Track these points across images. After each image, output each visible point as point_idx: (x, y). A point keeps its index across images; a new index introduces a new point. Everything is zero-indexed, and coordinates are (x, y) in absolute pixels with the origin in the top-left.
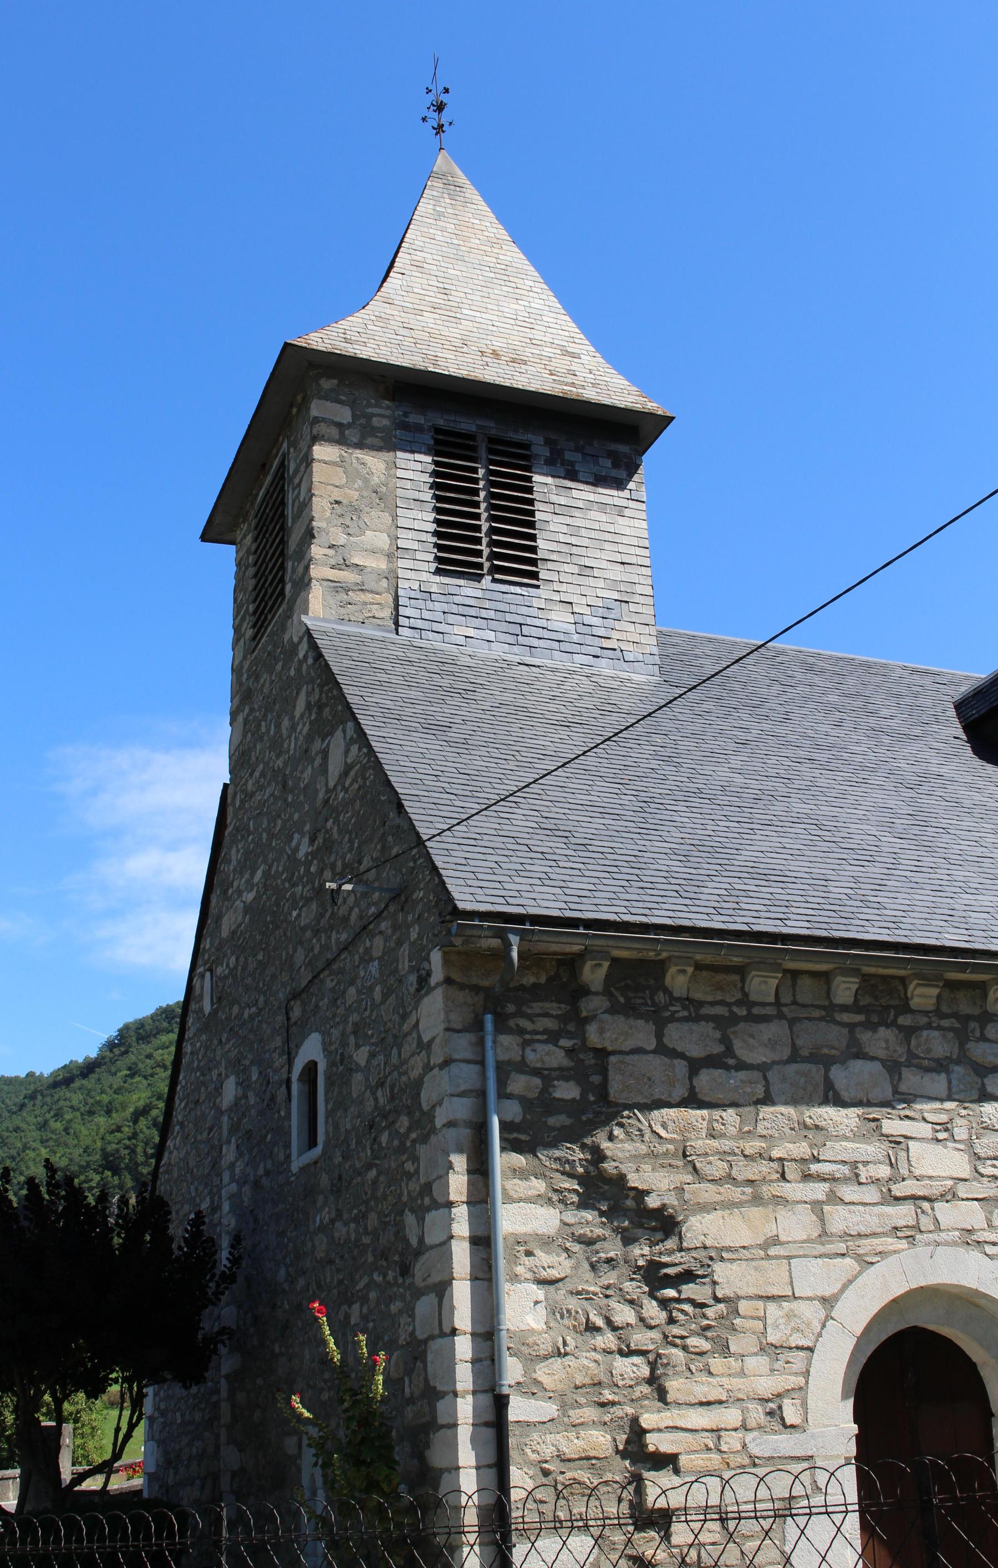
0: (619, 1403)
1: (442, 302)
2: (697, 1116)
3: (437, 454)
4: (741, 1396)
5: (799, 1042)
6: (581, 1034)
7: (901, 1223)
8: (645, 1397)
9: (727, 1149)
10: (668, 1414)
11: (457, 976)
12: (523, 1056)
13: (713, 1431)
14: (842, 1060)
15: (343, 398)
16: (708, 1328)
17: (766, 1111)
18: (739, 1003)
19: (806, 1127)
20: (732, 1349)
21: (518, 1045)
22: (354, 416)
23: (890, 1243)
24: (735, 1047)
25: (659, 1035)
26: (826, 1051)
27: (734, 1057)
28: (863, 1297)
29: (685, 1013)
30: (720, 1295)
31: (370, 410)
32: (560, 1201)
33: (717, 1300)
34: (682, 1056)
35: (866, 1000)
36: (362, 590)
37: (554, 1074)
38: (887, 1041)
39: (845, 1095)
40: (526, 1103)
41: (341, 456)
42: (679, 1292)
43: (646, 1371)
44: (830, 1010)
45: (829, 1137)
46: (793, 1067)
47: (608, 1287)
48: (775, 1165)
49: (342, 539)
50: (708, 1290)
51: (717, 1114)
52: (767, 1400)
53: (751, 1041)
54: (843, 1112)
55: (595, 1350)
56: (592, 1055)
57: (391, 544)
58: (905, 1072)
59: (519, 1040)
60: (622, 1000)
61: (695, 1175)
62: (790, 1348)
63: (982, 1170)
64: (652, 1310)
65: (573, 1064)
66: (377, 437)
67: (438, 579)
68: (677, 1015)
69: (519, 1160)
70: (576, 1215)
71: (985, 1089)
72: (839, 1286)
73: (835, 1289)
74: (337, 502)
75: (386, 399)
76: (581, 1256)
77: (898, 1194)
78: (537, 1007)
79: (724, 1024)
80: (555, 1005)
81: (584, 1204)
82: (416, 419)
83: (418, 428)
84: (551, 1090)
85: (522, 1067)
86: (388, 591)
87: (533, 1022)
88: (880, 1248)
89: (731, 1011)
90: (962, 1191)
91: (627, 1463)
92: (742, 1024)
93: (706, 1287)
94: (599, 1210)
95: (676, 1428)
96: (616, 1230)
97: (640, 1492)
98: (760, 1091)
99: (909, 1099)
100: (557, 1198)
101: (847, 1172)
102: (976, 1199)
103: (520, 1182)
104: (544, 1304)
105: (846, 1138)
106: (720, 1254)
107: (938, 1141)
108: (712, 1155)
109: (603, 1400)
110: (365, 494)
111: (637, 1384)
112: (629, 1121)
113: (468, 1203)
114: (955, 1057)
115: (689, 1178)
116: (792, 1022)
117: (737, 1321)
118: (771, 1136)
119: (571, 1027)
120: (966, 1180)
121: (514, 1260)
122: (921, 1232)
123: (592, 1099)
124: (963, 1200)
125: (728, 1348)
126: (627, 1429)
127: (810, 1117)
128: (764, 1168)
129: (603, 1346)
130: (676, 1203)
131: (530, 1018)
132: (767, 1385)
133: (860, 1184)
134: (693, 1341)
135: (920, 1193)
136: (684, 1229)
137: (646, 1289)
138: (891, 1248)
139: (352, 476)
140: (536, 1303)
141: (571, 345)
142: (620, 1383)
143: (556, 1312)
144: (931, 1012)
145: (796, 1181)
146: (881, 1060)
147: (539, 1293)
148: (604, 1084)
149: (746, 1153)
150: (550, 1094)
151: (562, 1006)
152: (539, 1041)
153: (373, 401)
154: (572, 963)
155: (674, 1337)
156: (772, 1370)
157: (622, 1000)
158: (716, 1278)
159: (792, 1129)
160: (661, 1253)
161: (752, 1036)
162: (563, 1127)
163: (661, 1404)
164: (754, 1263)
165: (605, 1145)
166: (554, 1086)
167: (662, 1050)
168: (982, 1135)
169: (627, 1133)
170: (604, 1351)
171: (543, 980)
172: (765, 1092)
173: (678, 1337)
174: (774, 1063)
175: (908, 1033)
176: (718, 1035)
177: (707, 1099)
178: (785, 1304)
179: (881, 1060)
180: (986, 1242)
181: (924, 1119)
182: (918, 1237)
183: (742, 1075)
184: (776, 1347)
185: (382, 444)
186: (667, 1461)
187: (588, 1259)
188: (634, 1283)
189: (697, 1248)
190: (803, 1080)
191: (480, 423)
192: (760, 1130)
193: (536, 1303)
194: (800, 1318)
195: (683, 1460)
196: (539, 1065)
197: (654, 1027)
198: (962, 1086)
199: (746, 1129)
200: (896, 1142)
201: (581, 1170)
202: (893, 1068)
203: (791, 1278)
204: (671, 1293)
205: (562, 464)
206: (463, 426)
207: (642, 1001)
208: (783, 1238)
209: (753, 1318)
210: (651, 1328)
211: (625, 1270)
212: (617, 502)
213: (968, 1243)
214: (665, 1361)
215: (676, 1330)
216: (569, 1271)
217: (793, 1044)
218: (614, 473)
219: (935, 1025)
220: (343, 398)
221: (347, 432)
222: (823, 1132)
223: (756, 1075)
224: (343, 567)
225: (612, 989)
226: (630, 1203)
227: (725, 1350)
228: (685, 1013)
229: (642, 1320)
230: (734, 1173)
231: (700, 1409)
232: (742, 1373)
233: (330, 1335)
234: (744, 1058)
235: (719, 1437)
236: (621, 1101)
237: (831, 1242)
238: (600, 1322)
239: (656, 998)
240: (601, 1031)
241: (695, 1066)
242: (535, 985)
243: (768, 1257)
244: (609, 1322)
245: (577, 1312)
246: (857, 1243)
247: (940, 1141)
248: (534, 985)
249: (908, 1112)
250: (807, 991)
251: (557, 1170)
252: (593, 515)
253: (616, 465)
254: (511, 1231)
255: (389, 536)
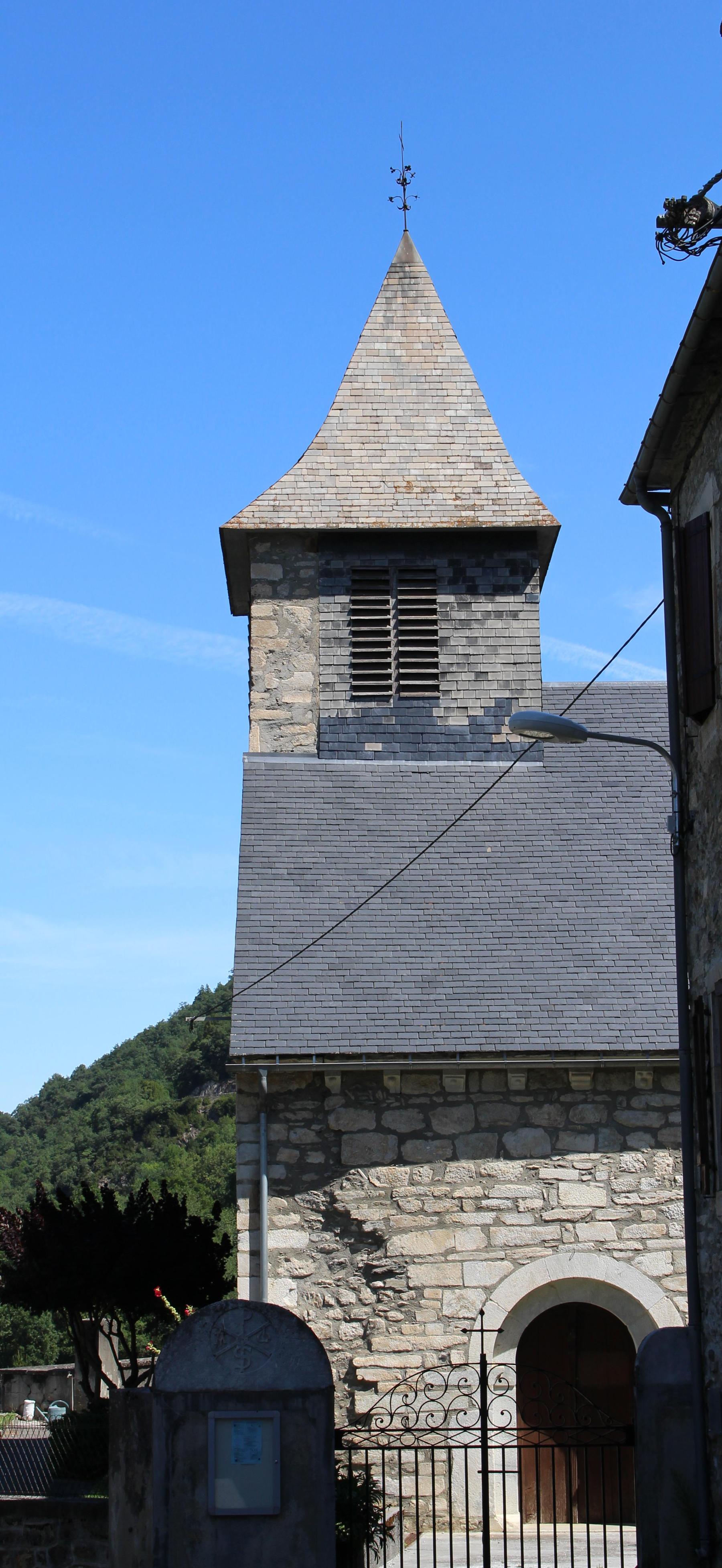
0: (342, 1350)
1: (371, 433)
2: (402, 1171)
3: (354, 592)
4: (421, 1348)
5: (481, 1118)
6: (325, 1121)
7: (549, 1237)
8: (359, 1347)
9: (421, 1192)
10: (372, 1358)
11: (245, 1088)
12: (288, 1137)
13: (401, 1368)
14: (514, 1129)
15: (275, 558)
16: (402, 1305)
17: (453, 1165)
18: (437, 1094)
19: (482, 1176)
20: (418, 1318)
21: (285, 1130)
22: (285, 573)
23: (539, 1251)
24: (433, 1124)
25: (378, 1120)
26: (501, 1123)
27: (432, 1130)
28: (515, 1286)
29: (397, 1104)
30: (411, 1285)
31: (298, 564)
32: (309, 1227)
33: (410, 1288)
34: (394, 1132)
35: (534, 1086)
36: (291, 724)
37: (309, 1147)
38: (549, 1114)
39: (513, 1152)
40: (288, 1166)
41: (274, 611)
42: (385, 1283)
43: (361, 1331)
44: (506, 1095)
45: (498, 1182)
46: (476, 1135)
47: (339, 1280)
48: (456, 1202)
49: (275, 683)
50: (404, 1281)
51: (416, 1169)
52: (441, 1351)
53: (445, 1119)
54: (511, 1164)
55: (328, 1318)
56: (332, 1134)
57: (315, 681)
58: (562, 1135)
59: (285, 1126)
60: (353, 1098)
61: (399, 1210)
62: (459, 1318)
63: (616, 1200)
64: (367, 1294)
65: (321, 1140)
66: (304, 587)
67: (353, 705)
68: (391, 1106)
69: (283, 1202)
70: (319, 1236)
71: (626, 1144)
72: (497, 1279)
73: (494, 1281)
74: (271, 652)
75: (310, 551)
76: (323, 1261)
77: (547, 1218)
78: (299, 1104)
79: (426, 1110)
80: (310, 1102)
81: (326, 1228)
82: (337, 564)
83: (339, 573)
84: (305, 1157)
85: (287, 1144)
86: (312, 721)
87: (295, 1114)
88: (531, 1255)
89: (431, 1100)
90: (599, 1215)
91: (346, 1386)
92: (440, 1109)
93: (402, 1280)
94: (335, 1233)
95: (377, 1366)
96: (346, 1245)
97: (353, 1403)
98: (449, 1153)
99: (563, 1152)
100: (306, 1225)
101: (510, 1205)
102: (611, 1220)
103: (283, 1216)
104: (296, 1291)
105: (511, 1182)
106: (414, 1259)
107: (583, 1181)
108: (411, 1197)
109: (332, 1348)
110: (294, 640)
111: (355, 1339)
112: (354, 1177)
113: (249, 1230)
114: (604, 1122)
115: (394, 1212)
116: (476, 1105)
117: (422, 1302)
118: (455, 1182)
119: (320, 1117)
120: (603, 1208)
121: (277, 1264)
122: (564, 1243)
123: (331, 1162)
124: (599, 1221)
125: (415, 1318)
126: (347, 1366)
127: (485, 1169)
128: (447, 1203)
129: (333, 1316)
130: (384, 1228)
131: (293, 1112)
132: (440, 1341)
133: (519, 1212)
134: (392, 1314)
135: (565, 1218)
136: (388, 1244)
137: (364, 1281)
138: (539, 1254)
139: (283, 625)
140: (291, 1290)
141: (487, 453)
142: (344, 1338)
143: (304, 1295)
144: (588, 1091)
145: (471, 1212)
146: (543, 1127)
147: (293, 1284)
148: (339, 1154)
149: (435, 1194)
150: (305, 1160)
151: (316, 1102)
152: (298, 1127)
153: (300, 555)
154: (320, 1075)
155: (379, 1311)
156: (445, 1332)
157: (353, 1098)
158: (409, 1274)
159: (470, 1177)
160: (373, 1259)
161: (446, 1117)
162: (313, 1181)
163: (368, 1352)
164: (436, 1265)
165: (337, 1192)
166: (308, 1155)
167: (381, 1129)
168: (619, 1176)
169: (353, 1185)
170: (334, 1319)
171: (303, 1086)
172: (453, 1153)
173: (381, 1311)
174: (461, 1133)
175: (568, 1106)
176: (421, 1116)
177: (410, 1160)
178: (457, 1291)
179: (543, 1127)
180: (615, 1249)
181: (573, 1166)
182: (561, 1247)
183: (437, 1143)
184: (449, 1318)
185: (308, 593)
186: (369, 1386)
187: (327, 1263)
188: (356, 1278)
189: (396, 1256)
190: (481, 1144)
191: (392, 557)
192: (447, 1178)
193: (291, 1290)
194: (467, 1299)
195: (380, 1386)
196: (298, 1142)
197: (375, 1115)
198: (606, 1143)
199: (437, 1178)
200: (548, 1183)
201: (323, 1208)
202: (553, 1132)
203: (463, 1274)
204: (379, 1284)
205: (464, 581)
206: (377, 563)
207: (366, 1098)
208: (459, 1249)
209: (433, 1299)
210: (366, 1305)
211: (350, 1269)
212: (513, 607)
213: (600, 1250)
214: (372, 1326)
215: (381, 1307)
216: (313, 1270)
217: (476, 1119)
218: (511, 581)
219: (589, 1100)
220: (275, 558)
221: (279, 588)
222: (493, 1179)
223: (446, 1142)
224: (276, 707)
225: (346, 1091)
226: (354, 1228)
227: (412, 1319)
228: (397, 1104)
229: (360, 1300)
230: (425, 1208)
231: (394, 1355)
232: (424, 1334)
233: (171, 1305)
234: (439, 1132)
235: (406, 1372)
236: (349, 1164)
237: (495, 1251)
238: (332, 1301)
239: (377, 1095)
240: (337, 1119)
241: (402, 1139)
242: (298, 1090)
243: (447, 1261)
244: (338, 1302)
245: (317, 1296)
246: (513, 1251)
247: (585, 1181)
248: (298, 1090)
249: (561, 1163)
250: (490, 1083)
251: (308, 1208)
252: (490, 623)
253: (513, 573)
254: (276, 1246)
255: (313, 674)
